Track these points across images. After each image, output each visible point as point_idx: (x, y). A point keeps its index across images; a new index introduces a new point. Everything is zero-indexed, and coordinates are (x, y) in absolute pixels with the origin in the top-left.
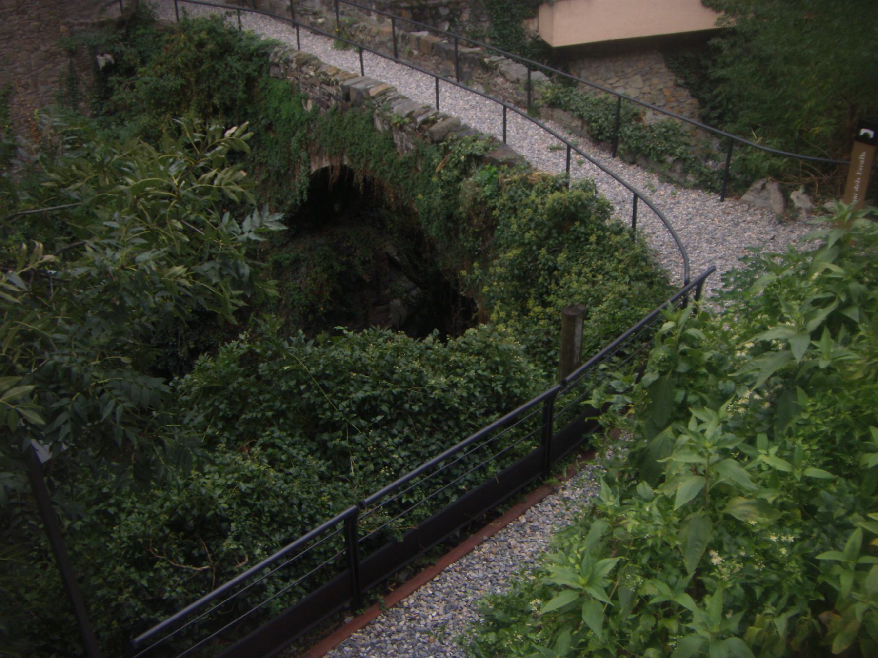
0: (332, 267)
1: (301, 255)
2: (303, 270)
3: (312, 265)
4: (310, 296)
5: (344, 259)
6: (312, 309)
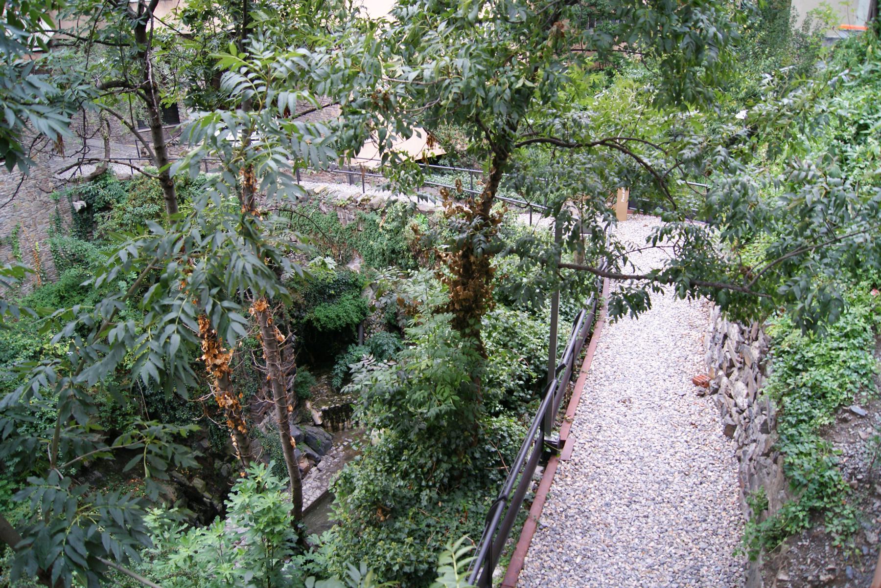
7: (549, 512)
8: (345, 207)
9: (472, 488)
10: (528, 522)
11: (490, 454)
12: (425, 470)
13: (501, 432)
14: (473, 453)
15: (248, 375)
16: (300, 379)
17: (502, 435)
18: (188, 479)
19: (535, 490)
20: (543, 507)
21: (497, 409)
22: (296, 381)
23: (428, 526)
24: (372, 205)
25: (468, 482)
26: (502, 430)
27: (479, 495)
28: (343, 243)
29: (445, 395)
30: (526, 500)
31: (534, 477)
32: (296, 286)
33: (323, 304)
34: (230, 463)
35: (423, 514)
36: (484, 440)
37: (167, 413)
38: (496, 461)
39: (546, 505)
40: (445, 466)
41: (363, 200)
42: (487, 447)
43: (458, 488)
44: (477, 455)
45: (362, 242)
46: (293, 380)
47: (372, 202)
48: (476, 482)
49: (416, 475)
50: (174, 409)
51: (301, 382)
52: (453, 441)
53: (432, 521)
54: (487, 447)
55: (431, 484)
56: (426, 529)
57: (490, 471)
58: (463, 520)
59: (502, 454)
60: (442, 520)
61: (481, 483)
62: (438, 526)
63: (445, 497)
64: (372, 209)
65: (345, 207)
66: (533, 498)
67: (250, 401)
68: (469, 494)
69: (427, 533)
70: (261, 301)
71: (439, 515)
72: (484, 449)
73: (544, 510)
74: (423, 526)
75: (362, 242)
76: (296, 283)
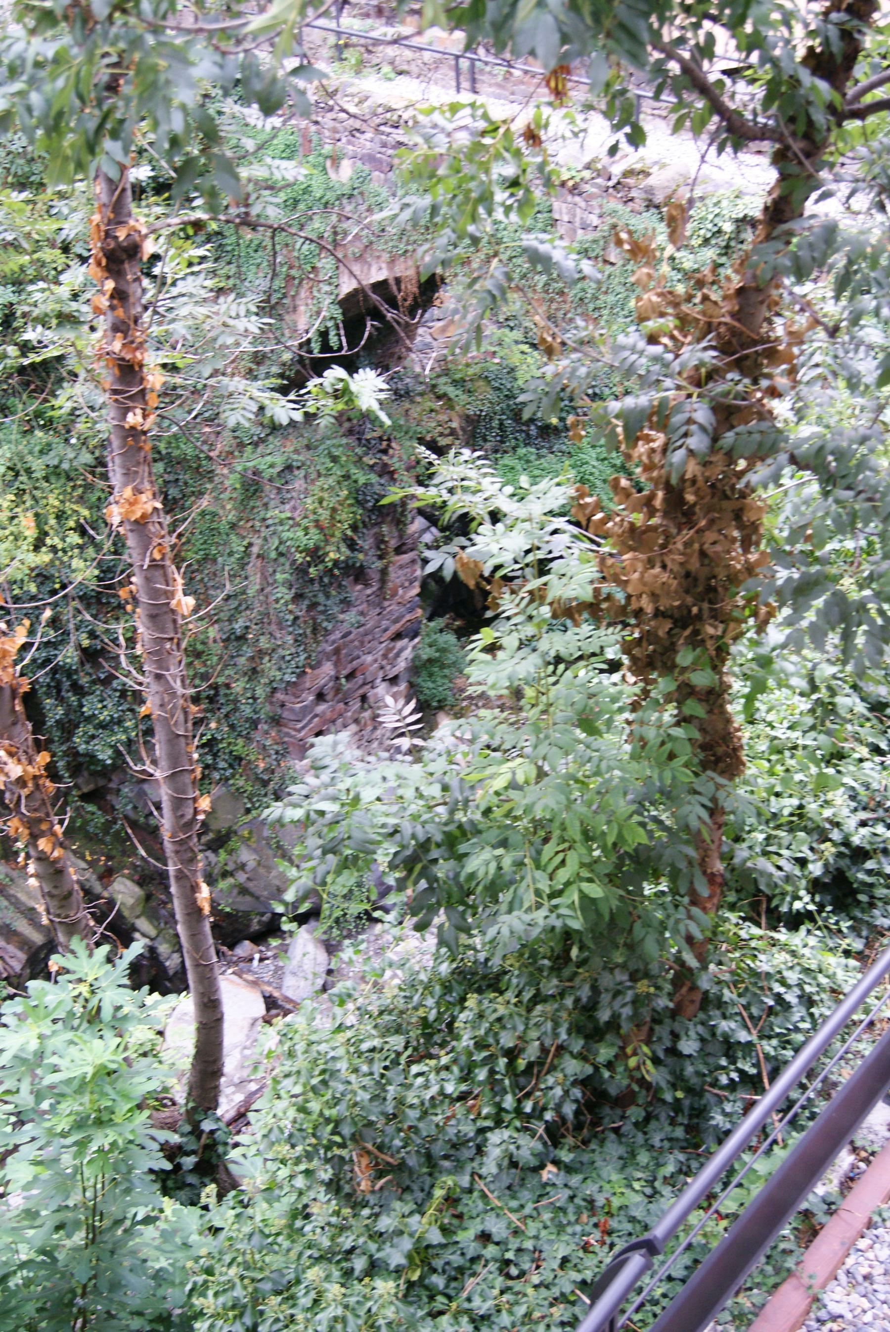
0: (347, 477)
1: (295, 457)
2: (298, 484)
3: (313, 476)
4: (313, 531)
5: (369, 460)
6: (315, 554)
7: (865, 1270)
8: (575, 190)
9: (656, 1141)
10: (785, 1288)
11: (730, 1048)
12: (522, 1063)
13: (778, 988)
14: (675, 1036)
15: (280, 624)
16: (427, 653)
17: (779, 998)
18: (101, 878)
19: (849, 1181)
20: (850, 1247)
21: (798, 905)
22: (417, 657)
23: (485, 1237)
24: (649, 191)
25: (648, 1118)
26: (783, 982)
27: (670, 1169)
28: (561, 293)
29: (563, 875)
30: (807, 1214)
31: (861, 1137)
32: (451, 391)
33: (522, 451)
34: (215, 851)
35: (484, 1196)
36: (720, 1004)
37: (61, 699)
38: (741, 1072)
39: (863, 1244)
40: (573, 1067)
41: (629, 173)
42: (725, 1026)
43: (616, 1130)
44: (688, 1046)
45: (611, 299)
46: (408, 653)
47: (651, 181)
48: (673, 1122)
49: (492, 1072)
50: (77, 689)
51: (430, 661)
52: (605, 998)
53: (497, 1227)
54: (725, 1026)
55: (528, 1107)
56: (472, 1249)
57: (720, 1100)
58: (593, 1239)
59: (767, 1057)
60: (532, 1228)
61: (689, 1129)
62: (514, 1244)
63: (566, 1156)
64: (650, 204)
65: (575, 190)
66: (831, 1213)
67: (280, 696)
68: (643, 1158)
69: (474, 1260)
70: (138, 491)
71: (528, 1210)
72: (713, 1030)
73: (850, 1261)
74: (466, 1237)
75: (611, 299)
76: (455, 383)
